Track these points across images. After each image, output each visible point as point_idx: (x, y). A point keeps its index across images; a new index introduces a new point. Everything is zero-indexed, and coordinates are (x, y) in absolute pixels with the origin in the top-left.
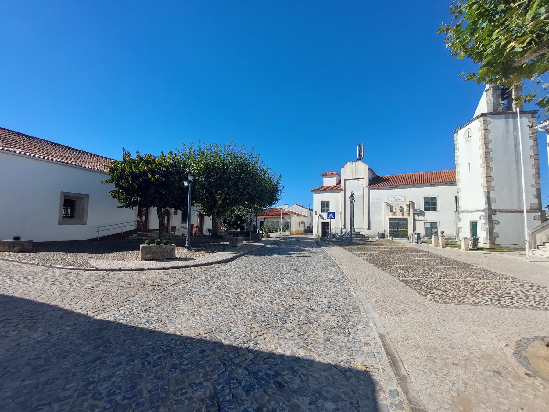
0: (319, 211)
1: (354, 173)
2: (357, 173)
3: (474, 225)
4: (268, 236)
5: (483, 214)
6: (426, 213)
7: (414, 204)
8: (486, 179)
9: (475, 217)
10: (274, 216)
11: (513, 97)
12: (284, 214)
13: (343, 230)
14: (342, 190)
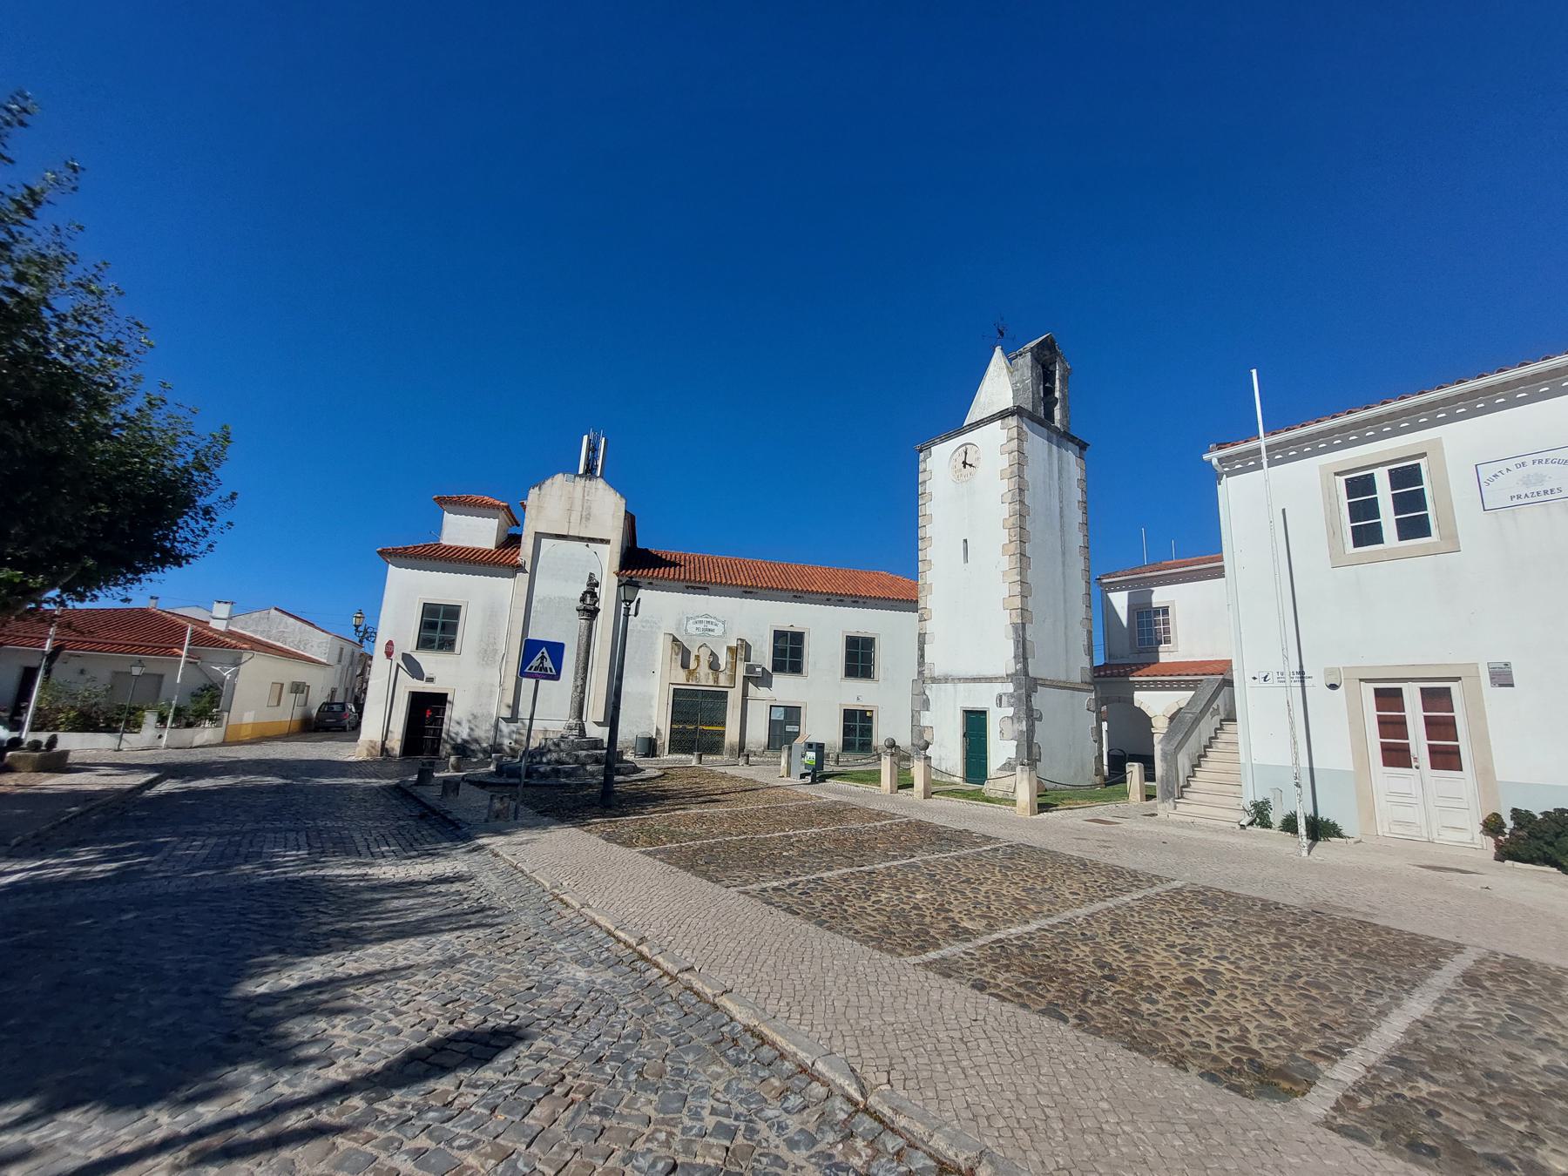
0: (408, 640)
1: (575, 517)
2: (586, 517)
3: (975, 723)
4: (58, 763)
5: (1010, 688)
6: (778, 679)
7: (747, 647)
9: (981, 697)
10: (132, 648)
11: (1057, 394)
12: (206, 640)
13: (503, 726)
14: (520, 568)
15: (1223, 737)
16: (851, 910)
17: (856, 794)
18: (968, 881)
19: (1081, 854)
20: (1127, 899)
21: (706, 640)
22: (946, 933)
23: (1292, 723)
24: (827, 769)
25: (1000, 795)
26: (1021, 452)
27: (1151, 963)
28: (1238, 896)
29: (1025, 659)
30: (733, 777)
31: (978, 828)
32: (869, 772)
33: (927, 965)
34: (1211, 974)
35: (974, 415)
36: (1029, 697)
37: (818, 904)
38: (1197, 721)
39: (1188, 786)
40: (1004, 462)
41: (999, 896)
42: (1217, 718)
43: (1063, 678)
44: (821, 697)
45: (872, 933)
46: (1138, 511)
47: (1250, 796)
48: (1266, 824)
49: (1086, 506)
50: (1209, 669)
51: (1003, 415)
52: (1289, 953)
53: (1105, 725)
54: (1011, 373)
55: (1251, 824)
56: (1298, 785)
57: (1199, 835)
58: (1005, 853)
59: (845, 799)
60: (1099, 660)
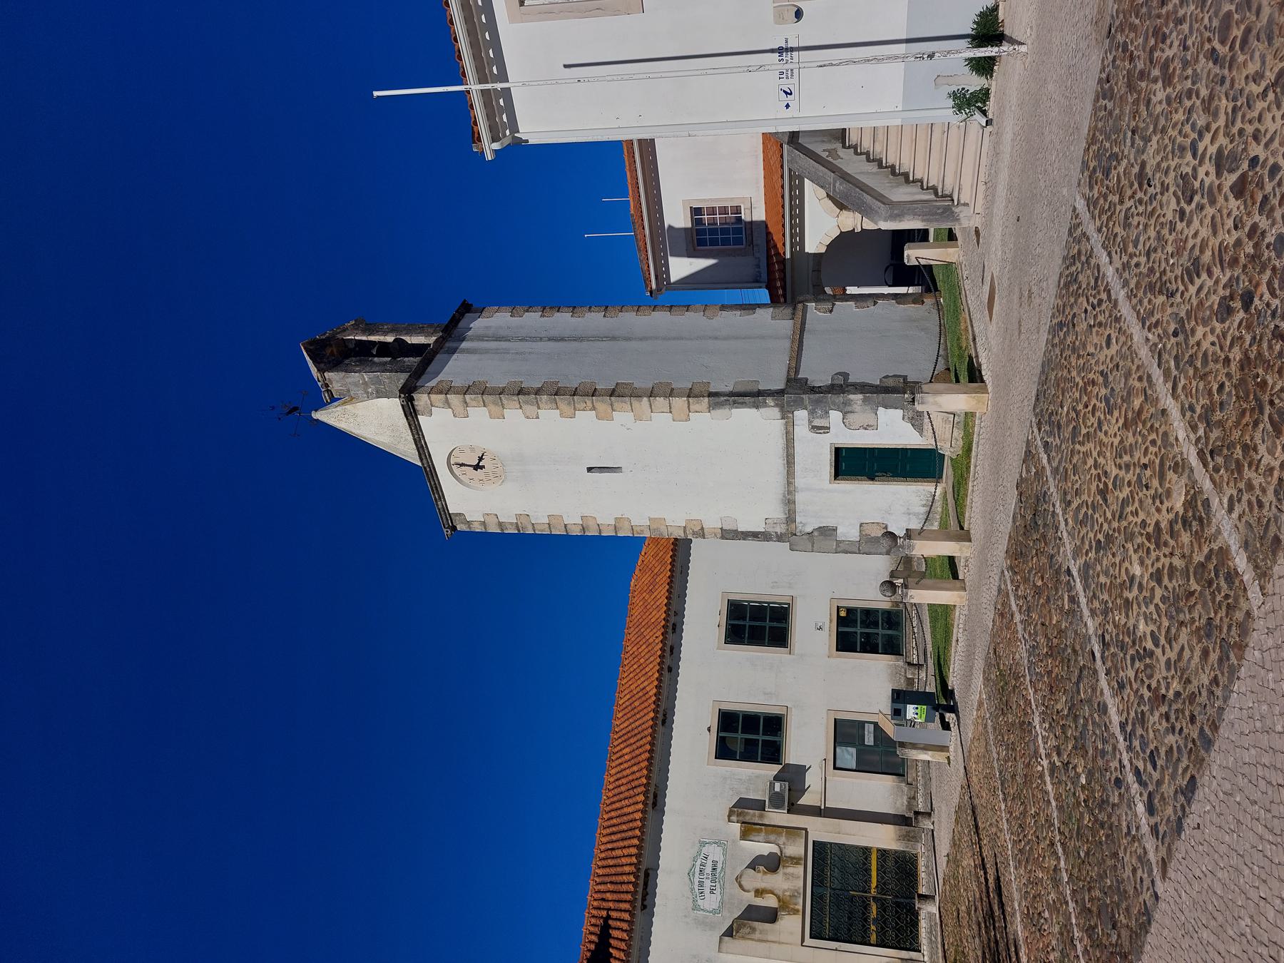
3: (852, 464)
5: (801, 415)
6: (794, 753)
7: (742, 805)
8: (660, 400)
9: (815, 453)
11: (390, 339)
15: (866, 145)
16: (1175, 686)
17: (971, 646)
18: (1103, 493)
19: (1045, 329)
20: (1110, 272)
21: (730, 876)
22: (1198, 536)
23: (848, 62)
24: (931, 688)
25: (958, 434)
26: (466, 391)
27: (1214, 242)
28: (1094, 129)
29: (760, 393)
30: (955, 844)
31: (1013, 468)
32: (934, 620)
33: (1263, 575)
34: (1222, 162)
35: (407, 451)
36: (813, 390)
37: (1171, 739)
38: (845, 177)
39: (934, 189)
40: (479, 414)
41: (1122, 450)
42: (842, 152)
43: (787, 344)
44: (817, 687)
45: (1214, 657)
46: (564, 235)
47: (945, 113)
48: (984, 95)
49: (549, 304)
50: (775, 159)
51: (411, 413)
52: (1177, 64)
53: (851, 290)
54: (352, 399)
55: (984, 113)
56: (931, 56)
57: (1004, 176)
58: (1051, 433)
59: (979, 664)
60: (763, 295)
